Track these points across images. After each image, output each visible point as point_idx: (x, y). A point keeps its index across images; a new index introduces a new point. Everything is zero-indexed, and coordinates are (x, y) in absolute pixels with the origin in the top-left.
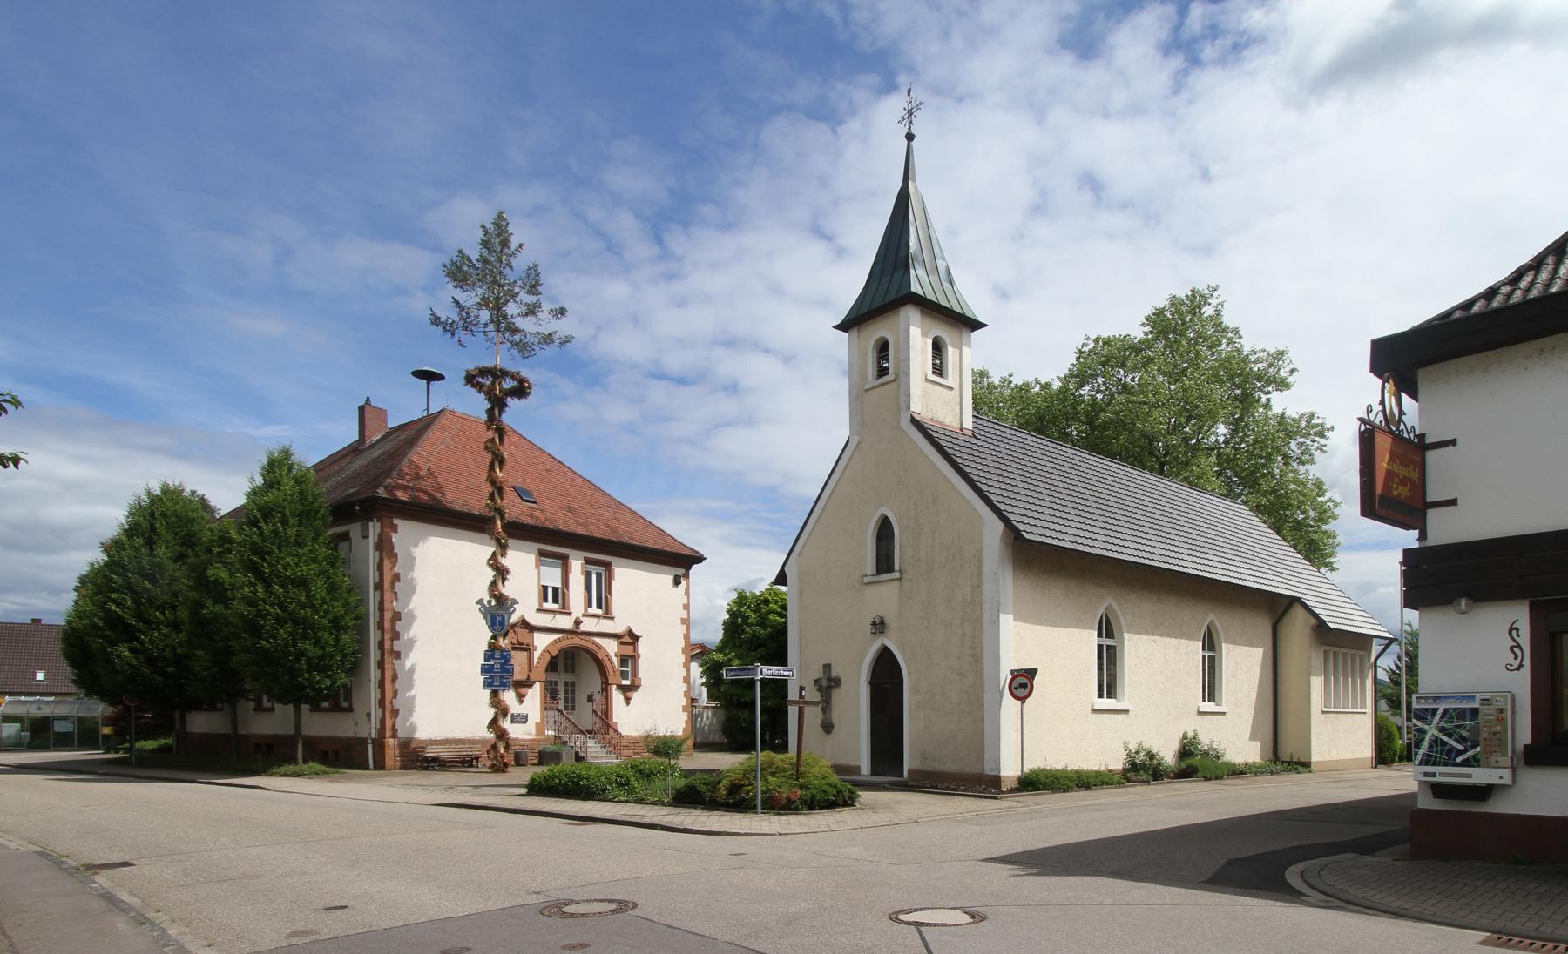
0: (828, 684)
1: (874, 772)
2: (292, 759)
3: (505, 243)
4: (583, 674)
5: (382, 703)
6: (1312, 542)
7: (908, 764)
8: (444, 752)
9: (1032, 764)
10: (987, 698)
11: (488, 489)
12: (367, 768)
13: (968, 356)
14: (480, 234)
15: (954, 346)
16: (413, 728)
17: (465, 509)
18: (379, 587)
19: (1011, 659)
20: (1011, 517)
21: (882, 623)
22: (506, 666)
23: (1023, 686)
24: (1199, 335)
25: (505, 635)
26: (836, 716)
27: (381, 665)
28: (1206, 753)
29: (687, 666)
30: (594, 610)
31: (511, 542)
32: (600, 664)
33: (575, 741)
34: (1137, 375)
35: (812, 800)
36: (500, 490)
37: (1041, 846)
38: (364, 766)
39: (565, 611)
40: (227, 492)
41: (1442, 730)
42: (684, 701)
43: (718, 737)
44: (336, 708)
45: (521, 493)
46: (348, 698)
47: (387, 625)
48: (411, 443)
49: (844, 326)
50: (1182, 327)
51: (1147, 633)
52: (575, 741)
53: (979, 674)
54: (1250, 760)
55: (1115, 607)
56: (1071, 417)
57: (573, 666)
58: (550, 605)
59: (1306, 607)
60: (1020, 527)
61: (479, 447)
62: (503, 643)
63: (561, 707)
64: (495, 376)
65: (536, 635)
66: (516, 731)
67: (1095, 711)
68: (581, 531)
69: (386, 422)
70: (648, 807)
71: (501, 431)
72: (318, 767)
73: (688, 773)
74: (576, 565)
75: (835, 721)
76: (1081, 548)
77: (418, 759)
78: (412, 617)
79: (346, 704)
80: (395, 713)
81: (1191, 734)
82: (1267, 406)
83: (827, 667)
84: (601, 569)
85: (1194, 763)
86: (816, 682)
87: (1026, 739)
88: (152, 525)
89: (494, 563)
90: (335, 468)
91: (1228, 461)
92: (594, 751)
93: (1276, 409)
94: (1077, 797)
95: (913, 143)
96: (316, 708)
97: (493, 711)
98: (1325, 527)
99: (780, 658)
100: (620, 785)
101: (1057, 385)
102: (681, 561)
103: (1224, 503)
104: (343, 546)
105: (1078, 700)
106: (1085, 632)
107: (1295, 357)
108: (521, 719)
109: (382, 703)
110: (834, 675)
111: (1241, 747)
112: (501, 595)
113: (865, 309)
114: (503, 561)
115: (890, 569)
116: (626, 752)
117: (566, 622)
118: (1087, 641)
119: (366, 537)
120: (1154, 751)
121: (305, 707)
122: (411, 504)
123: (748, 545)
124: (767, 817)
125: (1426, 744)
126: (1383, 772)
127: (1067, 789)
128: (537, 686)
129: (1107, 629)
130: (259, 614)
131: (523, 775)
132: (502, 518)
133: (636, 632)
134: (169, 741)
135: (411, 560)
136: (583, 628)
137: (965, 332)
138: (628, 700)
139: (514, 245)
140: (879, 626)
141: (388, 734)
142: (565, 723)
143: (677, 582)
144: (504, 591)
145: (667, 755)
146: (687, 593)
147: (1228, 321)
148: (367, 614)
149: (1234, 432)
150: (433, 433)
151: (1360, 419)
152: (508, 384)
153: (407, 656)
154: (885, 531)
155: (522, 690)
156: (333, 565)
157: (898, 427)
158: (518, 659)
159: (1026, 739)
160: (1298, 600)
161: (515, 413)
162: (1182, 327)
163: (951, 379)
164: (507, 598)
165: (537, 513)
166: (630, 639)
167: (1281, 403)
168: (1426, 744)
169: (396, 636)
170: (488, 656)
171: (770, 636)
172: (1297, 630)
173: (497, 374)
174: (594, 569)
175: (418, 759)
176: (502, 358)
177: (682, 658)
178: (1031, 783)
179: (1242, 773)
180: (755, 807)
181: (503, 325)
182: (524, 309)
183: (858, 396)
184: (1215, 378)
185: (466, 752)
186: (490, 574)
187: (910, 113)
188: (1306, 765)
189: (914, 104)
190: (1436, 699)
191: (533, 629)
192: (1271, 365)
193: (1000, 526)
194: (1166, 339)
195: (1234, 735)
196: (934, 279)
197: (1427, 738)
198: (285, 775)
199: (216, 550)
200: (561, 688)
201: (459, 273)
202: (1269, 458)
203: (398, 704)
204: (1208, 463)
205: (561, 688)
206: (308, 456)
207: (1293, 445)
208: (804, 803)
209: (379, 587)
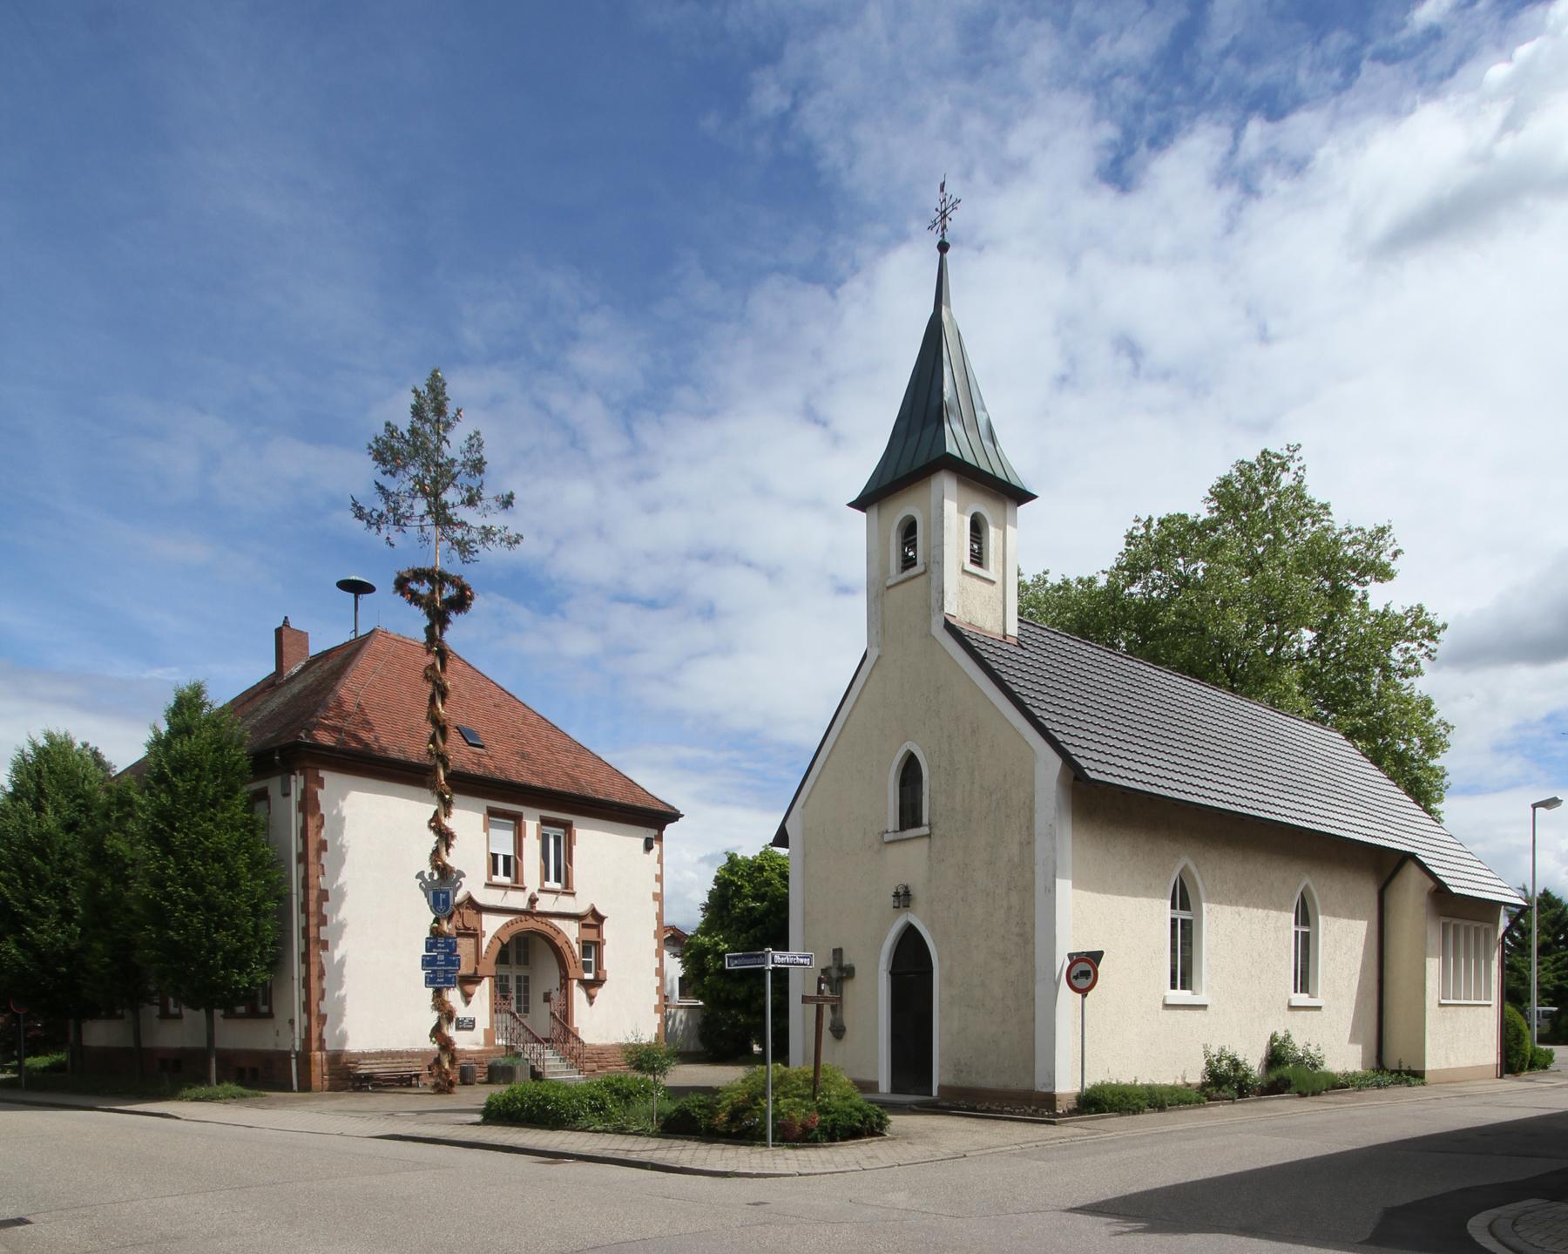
0: (838, 975)
1: (896, 1088)
2: (203, 1079)
3: (440, 410)
4: (538, 964)
5: (307, 1007)
6: (1417, 780)
8: (378, 1068)
9: (1094, 1078)
10: (1039, 990)
11: (429, 729)
12: (290, 1090)
14: (412, 399)
15: (996, 526)
16: (343, 1038)
17: (402, 756)
18: (303, 858)
19: (1069, 939)
20: (1072, 750)
21: (907, 894)
22: (452, 959)
23: (1085, 974)
24: (1275, 508)
25: (450, 918)
26: (848, 1018)
27: (306, 958)
29: (659, 954)
30: (552, 884)
31: (457, 798)
32: (558, 953)
33: (530, 1051)
34: (1201, 564)
35: (834, 1128)
36: (443, 730)
37: (1134, 1189)
38: (287, 1087)
39: (518, 886)
40: (123, 745)
42: (656, 1000)
43: (694, 1045)
44: (254, 1014)
45: (467, 735)
46: (268, 1000)
47: (312, 907)
48: (338, 673)
49: (861, 504)
50: (1255, 500)
51: (1230, 903)
52: (530, 1051)
53: (1029, 959)
54: (1350, 1070)
55: (1193, 868)
56: (1118, 623)
57: (527, 955)
58: (500, 878)
59: (1423, 867)
60: (1083, 763)
61: (416, 676)
62: (447, 927)
63: (513, 1009)
64: (431, 580)
65: (485, 917)
66: (465, 1041)
67: (1167, 1006)
68: (536, 782)
69: (307, 648)
70: (632, 1139)
71: (443, 654)
72: (234, 1089)
73: (676, 1092)
74: (531, 826)
76: (1155, 790)
77: (351, 1078)
78: (341, 895)
79: (264, 1009)
80: (323, 1019)
81: (1281, 1035)
82: (1363, 604)
83: (838, 953)
84: (560, 831)
85: (1286, 1074)
87: (1094, 1042)
88: (38, 786)
89: (437, 826)
90: (249, 708)
91: (1314, 675)
92: (554, 1066)
93: (1375, 604)
94: (1148, 1123)
95: (948, 255)
96: (230, 1014)
97: (436, 1014)
98: (1432, 763)
99: (782, 943)
100: (594, 1109)
101: (1102, 582)
102: (652, 819)
103: (1314, 729)
104: (260, 807)
105: (1160, 992)
107: (1400, 536)
108: (467, 1025)
109: (307, 1007)
110: (846, 962)
111: (1342, 1054)
112: (446, 866)
114: (447, 822)
115: (917, 823)
116: (589, 1066)
117: (518, 900)
118: (1160, 912)
119: (287, 794)
120: (1240, 1058)
121: (218, 1013)
122: (341, 752)
123: (725, 803)
124: (779, 1151)
126: (1510, 1084)
127: (1137, 1110)
128: (486, 982)
129: (1182, 898)
130: (168, 897)
131: (480, 1095)
132: (446, 766)
133: (602, 912)
134: (61, 1057)
135: (340, 820)
136: (539, 907)
138: (591, 998)
139: (450, 411)
140: (903, 898)
141: (315, 1045)
142: (519, 1029)
143: (648, 847)
144: (448, 861)
145: (652, 1070)
146: (660, 860)
147: (1315, 492)
148: (290, 894)
149: (1320, 638)
150: (363, 661)
152: (449, 592)
153: (336, 946)
154: (910, 772)
155: (469, 988)
156: (252, 832)
157: (929, 635)
158: (465, 947)
159: (1094, 1042)
160: (1412, 856)
161: (458, 633)
162: (1255, 500)
163: (993, 571)
164: (452, 870)
165: (486, 760)
166: (593, 920)
167: (1377, 596)
169: (323, 921)
170: (431, 945)
171: (767, 912)
172: (1410, 896)
173: (437, 578)
174: (553, 832)
175: (351, 1078)
176: (441, 557)
177: (654, 944)
178: (1095, 1103)
179: (1343, 1086)
181: (442, 517)
182: (466, 495)
183: (879, 593)
184: (1302, 568)
185: (404, 1068)
186: (432, 839)
188: (1415, 1075)
191: (481, 909)
192: (1369, 547)
193: (1056, 762)
194: (1236, 518)
195: (1333, 1039)
196: (973, 437)
198: (197, 1099)
199: (114, 815)
200: (512, 984)
201: (387, 454)
202: (1365, 669)
203: (325, 1007)
204: (1291, 674)
205: (512, 984)
206: (220, 695)
207: (1395, 653)
208: (823, 1130)
209: (303, 858)
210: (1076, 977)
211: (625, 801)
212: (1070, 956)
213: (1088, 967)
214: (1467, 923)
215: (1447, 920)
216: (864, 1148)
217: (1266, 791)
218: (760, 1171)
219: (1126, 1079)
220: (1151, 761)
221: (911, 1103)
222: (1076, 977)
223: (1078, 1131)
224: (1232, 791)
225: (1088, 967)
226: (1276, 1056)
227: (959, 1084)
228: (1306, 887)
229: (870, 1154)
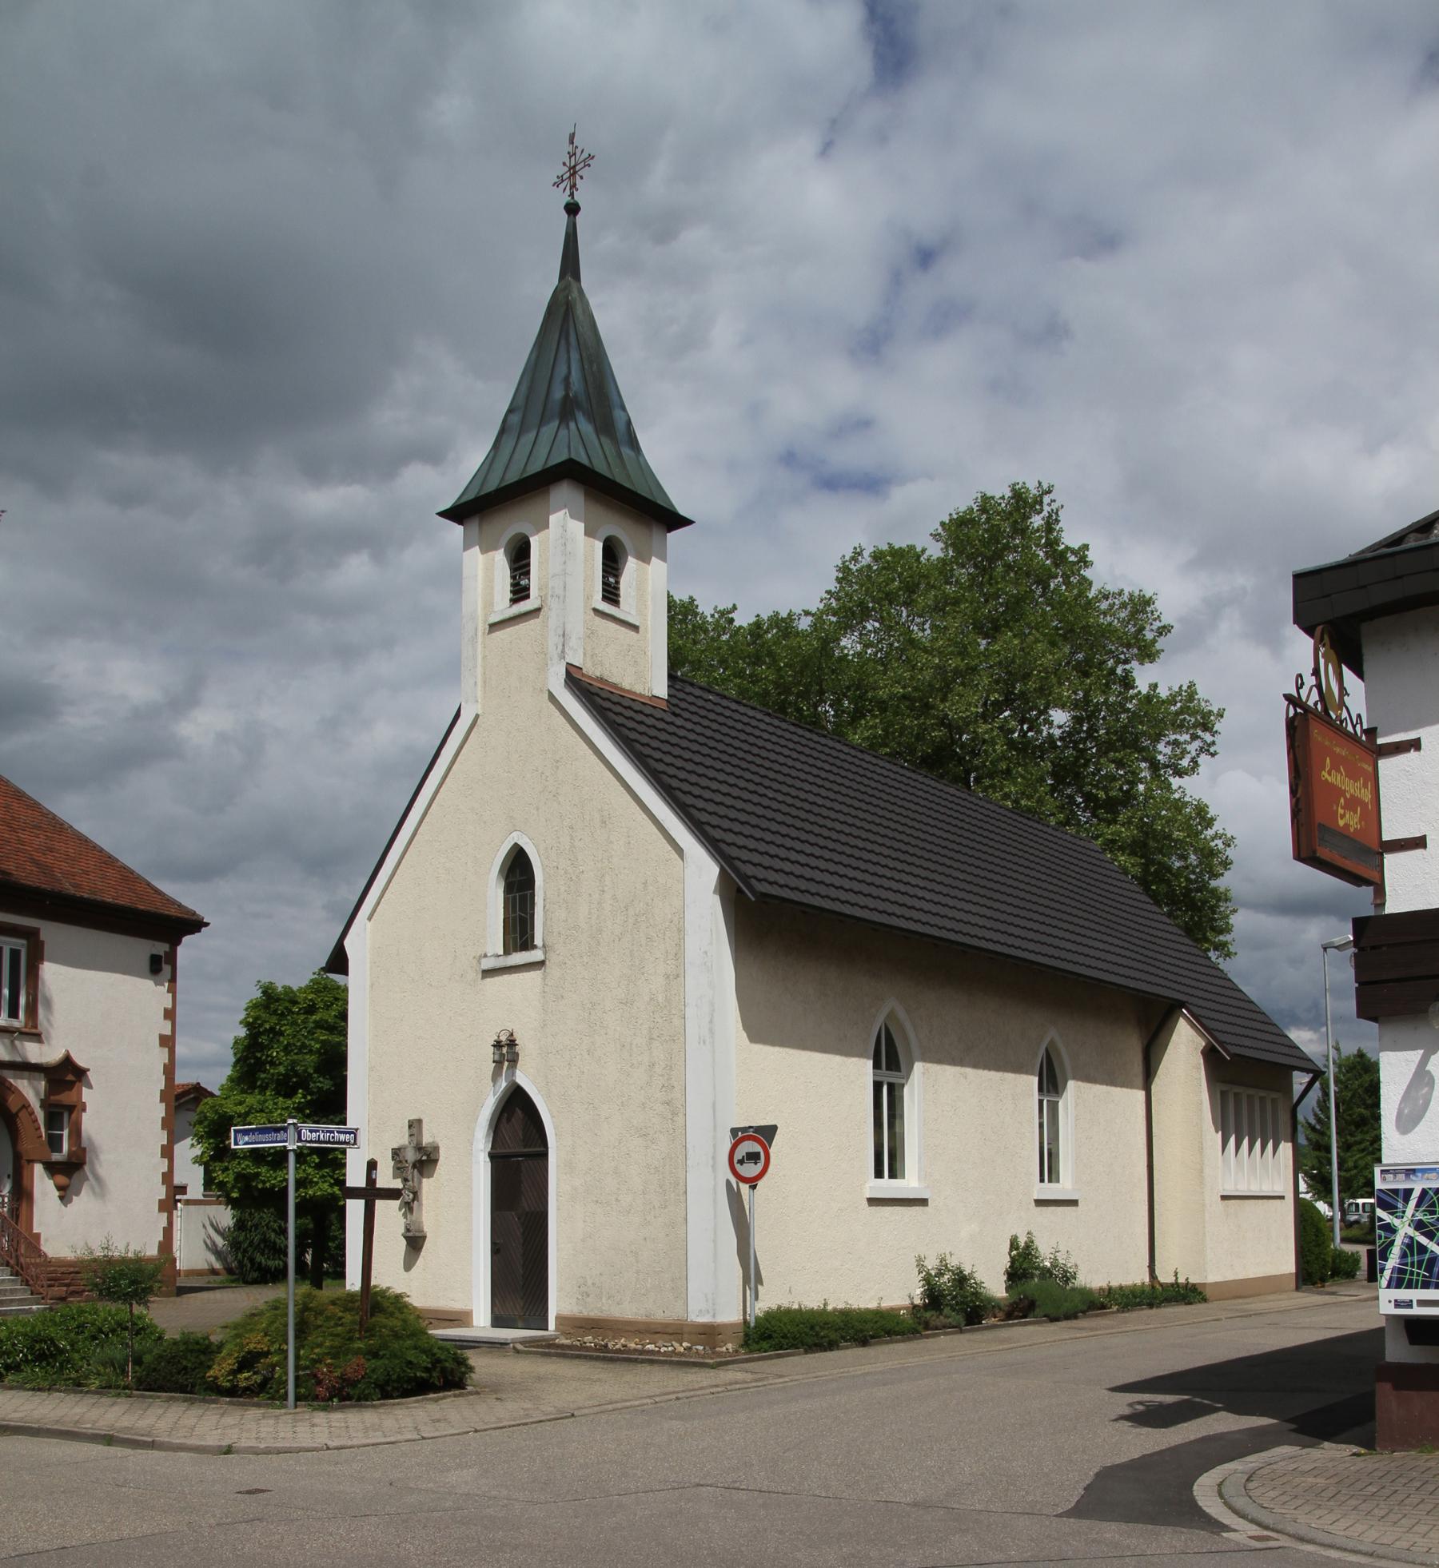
1: (498, 1321)
7: (558, 1303)
13: (648, 583)
23: (753, 1157)
28: (1047, 1273)
41: (1419, 1226)
54: (1138, 1282)
55: (902, 1015)
75: (428, 1228)
83: (415, 1125)
84: (20, 944)
86: (396, 1153)
94: (848, 1360)
106: (1025, 1077)
113: (492, 485)
115: (527, 944)
124: (304, 1412)
125: (1396, 1251)
127: (831, 1346)
133: (81, 1061)
137: (656, 532)
140: (506, 1051)
145: (127, 1298)
151: (1288, 697)
154: (518, 872)
163: (627, 608)
166: (66, 1076)
168: (1396, 1251)
179: (1103, 1307)
180: (285, 1397)
187: (573, 171)
189: (580, 157)
190: (1410, 1172)
197: (1399, 1240)
210: (741, 1162)
211: (120, 902)
212: (734, 1131)
213: (757, 1148)
214: (1251, 1091)
215: (1225, 1087)
216: (432, 1407)
217: (1055, 932)
218: (271, 1444)
219: (812, 1303)
220: (842, 870)
221: (514, 1341)
222: (741, 1162)
223: (740, 1376)
224: (1017, 931)
225: (757, 1148)
226: (1022, 1264)
227: (585, 1314)
228: (1052, 1042)
229: (437, 1416)
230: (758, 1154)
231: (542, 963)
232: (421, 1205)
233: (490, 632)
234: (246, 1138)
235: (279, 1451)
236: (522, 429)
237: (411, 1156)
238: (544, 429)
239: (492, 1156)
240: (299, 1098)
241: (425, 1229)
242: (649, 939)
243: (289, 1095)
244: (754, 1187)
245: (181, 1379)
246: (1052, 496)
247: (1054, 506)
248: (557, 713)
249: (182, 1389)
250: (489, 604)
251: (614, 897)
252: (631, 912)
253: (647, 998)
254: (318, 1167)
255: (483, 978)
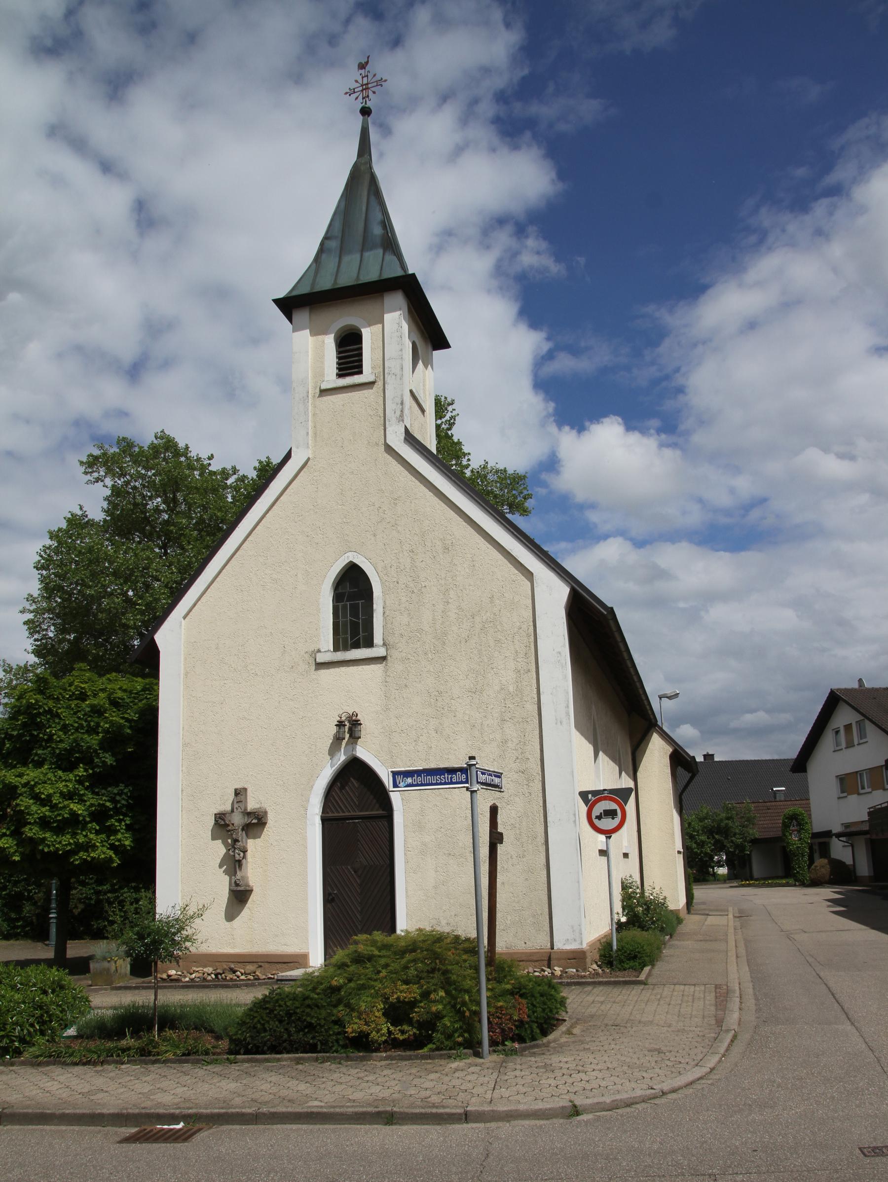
23: (611, 814)
83: (240, 793)
210: (599, 817)
213: (613, 806)
222: (599, 817)
225: (613, 806)
230: (615, 811)
231: (384, 658)
232: (247, 862)
233: (320, 396)
234: (409, 780)
235: (629, 1104)
236: (342, 251)
237: (237, 820)
238: (346, 259)
239: (324, 820)
240: (81, 771)
241: (251, 883)
242: (498, 641)
243: (70, 767)
244: (609, 838)
245: (309, 1039)
246: (453, 407)
247: (454, 413)
248: (394, 462)
249: (313, 1049)
250: (320, 374)
251: (459, 608)
252: (478, 619)
253: (497, 688)
254: (97, 833)
255: (316, 669)
